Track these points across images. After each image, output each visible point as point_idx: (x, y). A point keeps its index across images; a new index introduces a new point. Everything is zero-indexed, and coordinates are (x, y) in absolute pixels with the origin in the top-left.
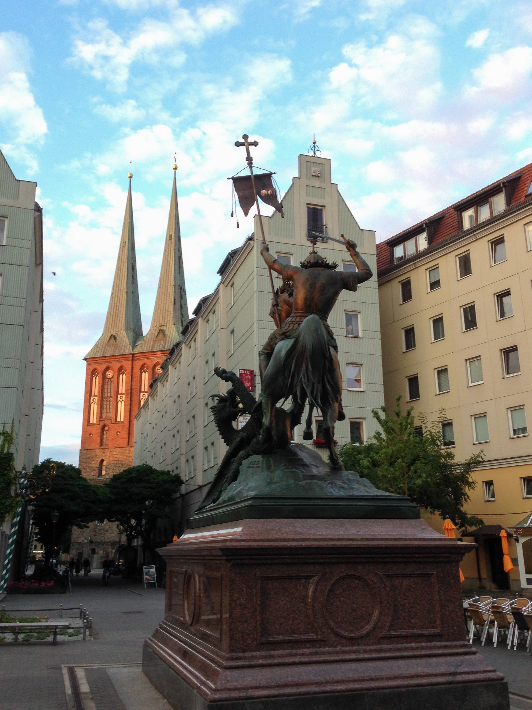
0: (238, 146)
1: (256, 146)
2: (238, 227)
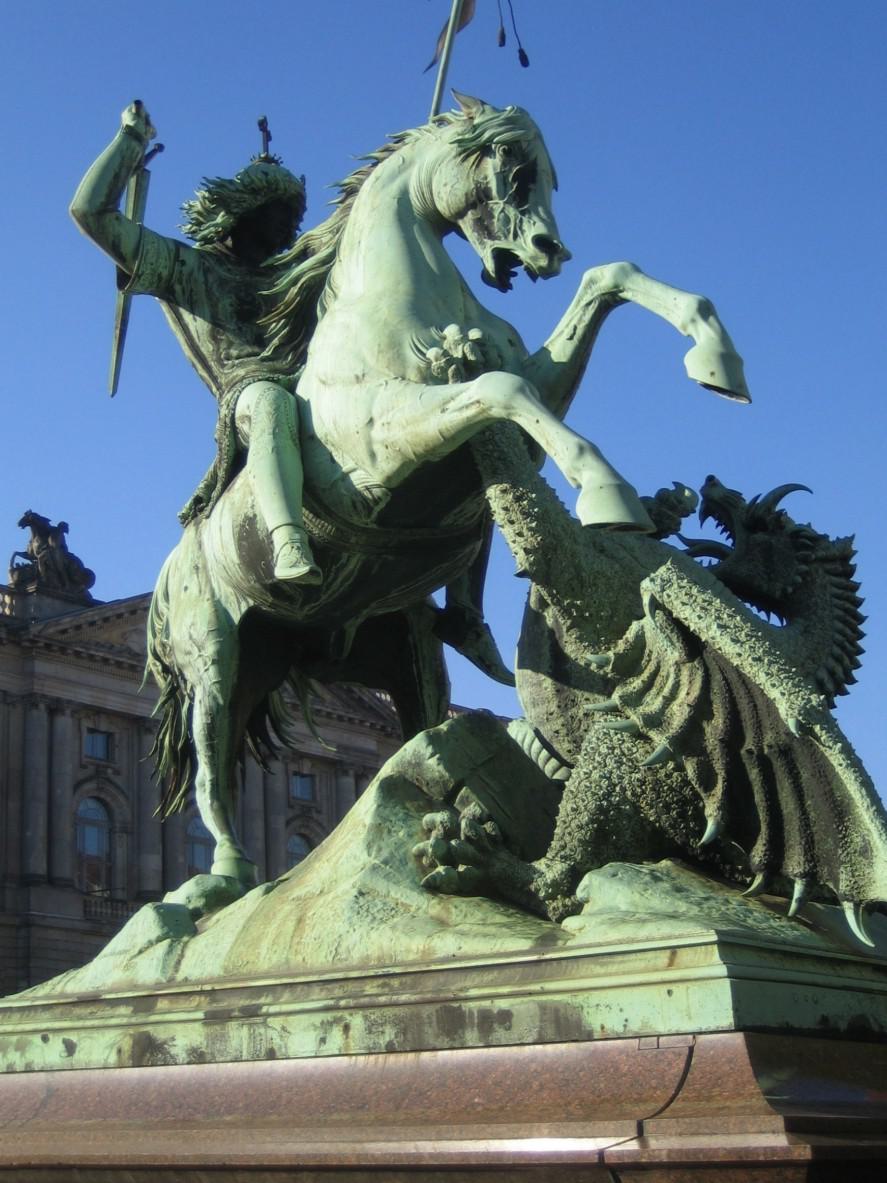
2: (263, 125)
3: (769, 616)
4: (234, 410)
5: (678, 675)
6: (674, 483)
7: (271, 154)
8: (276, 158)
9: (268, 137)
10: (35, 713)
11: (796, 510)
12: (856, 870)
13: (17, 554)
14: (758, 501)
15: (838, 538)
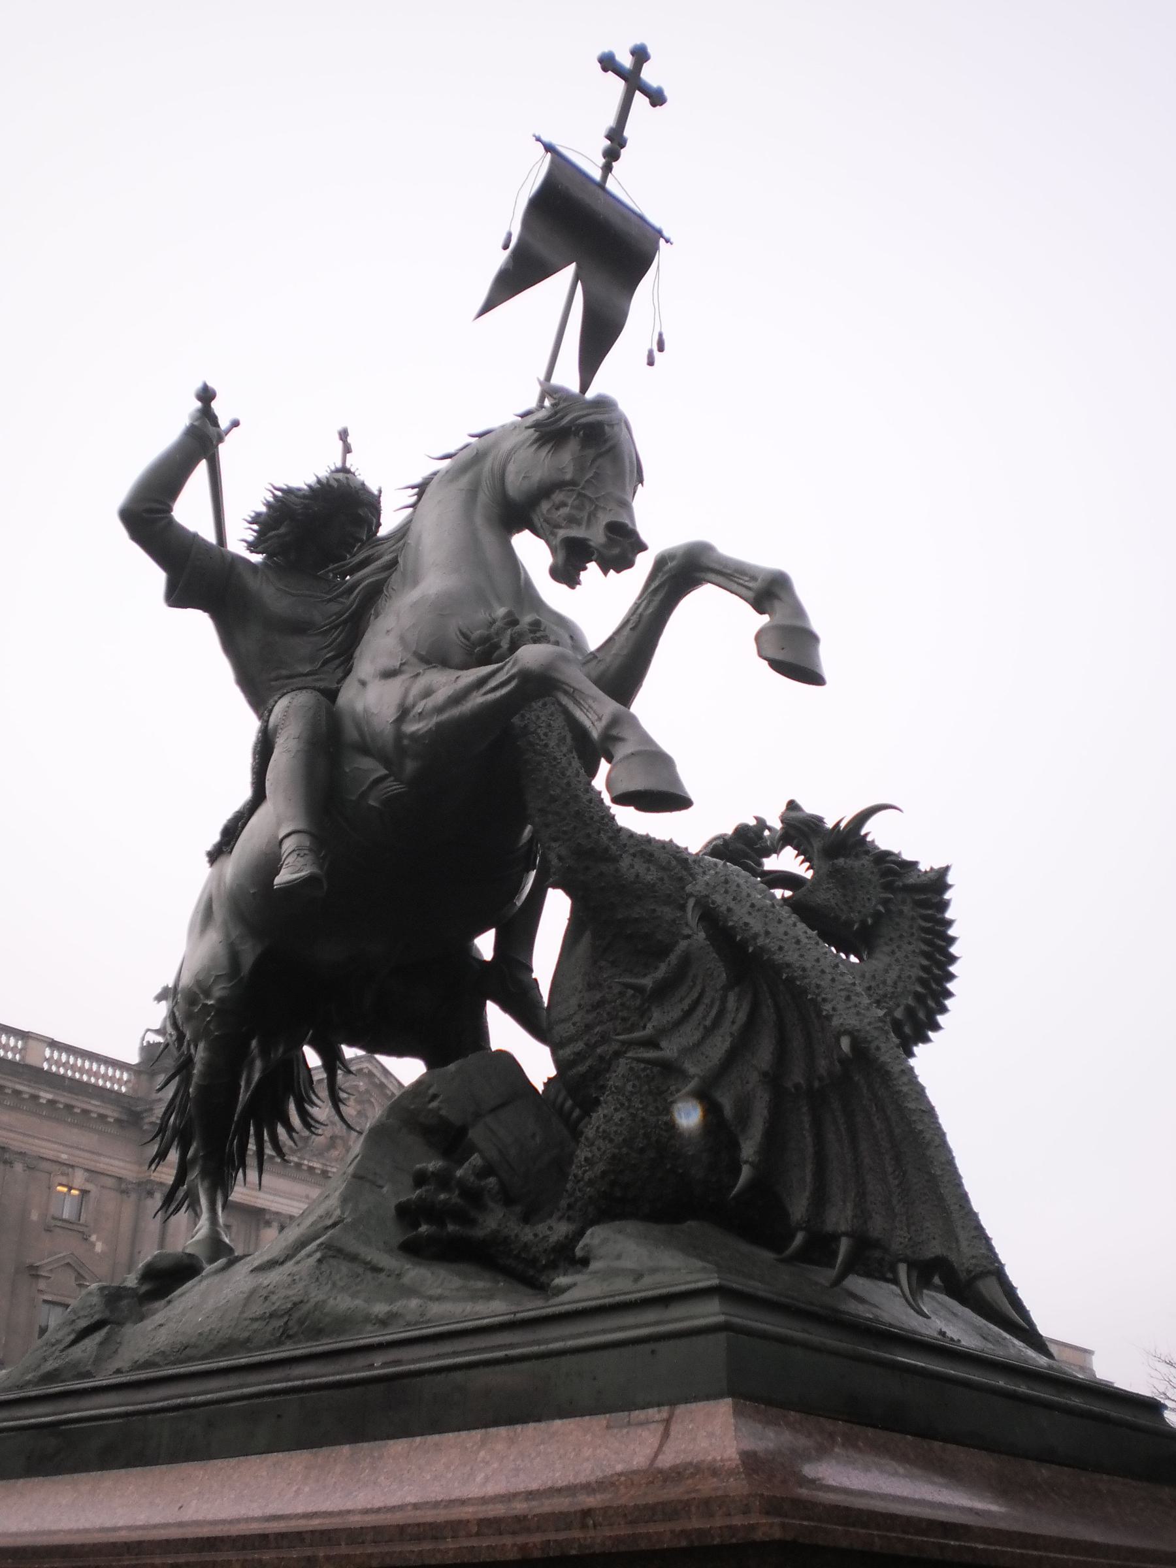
0: (605, 70)
1: (654, 104)
2: (343, 435)
3: (847, 957)
4: (267, 721)
5: (724, 1000)
6: (757, 818)
7: (348, 465)
9: (347, 449)
10: (149, 1202)
11: (882, 834)
12: (914, 1224)
13: (148, 1030)
15: (932, 869)
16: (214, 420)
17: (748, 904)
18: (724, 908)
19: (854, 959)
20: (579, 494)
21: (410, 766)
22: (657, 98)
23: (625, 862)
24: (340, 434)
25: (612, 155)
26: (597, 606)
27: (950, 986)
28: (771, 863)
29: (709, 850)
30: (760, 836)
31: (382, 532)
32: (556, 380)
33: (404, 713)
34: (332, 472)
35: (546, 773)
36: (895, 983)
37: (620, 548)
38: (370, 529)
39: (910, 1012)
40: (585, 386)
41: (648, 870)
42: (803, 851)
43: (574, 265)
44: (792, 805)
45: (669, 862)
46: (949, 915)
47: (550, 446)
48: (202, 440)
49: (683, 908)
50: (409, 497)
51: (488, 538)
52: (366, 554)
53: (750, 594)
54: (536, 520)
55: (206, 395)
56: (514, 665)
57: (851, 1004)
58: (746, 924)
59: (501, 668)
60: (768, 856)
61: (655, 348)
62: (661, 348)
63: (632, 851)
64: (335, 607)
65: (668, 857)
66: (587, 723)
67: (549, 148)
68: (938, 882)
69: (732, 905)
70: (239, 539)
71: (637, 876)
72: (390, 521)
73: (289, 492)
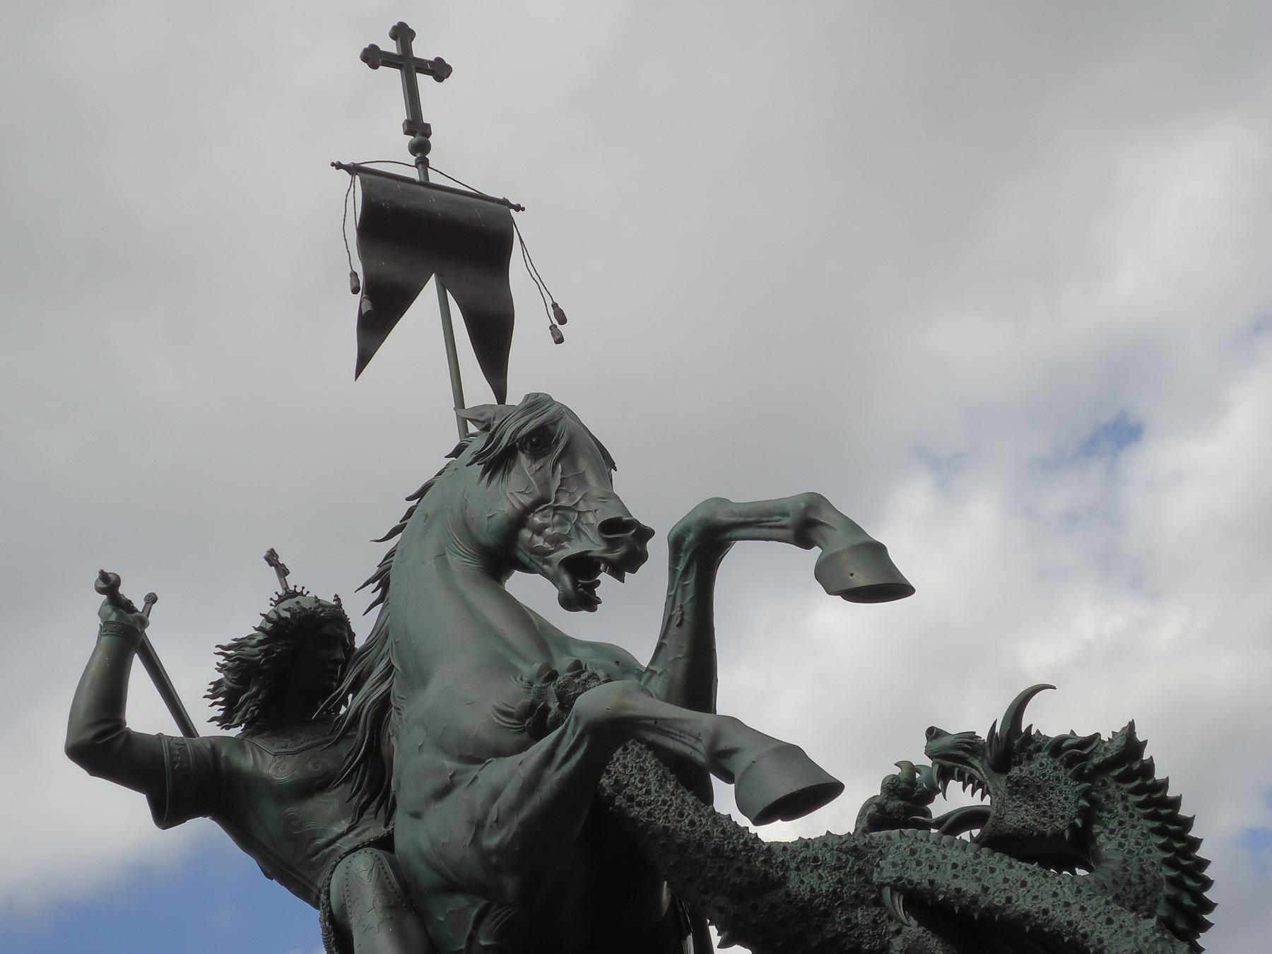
2: (272, 558)
8: (298, 590)
9: (283, 572)
11: (1046, 721)
14: (997, 730)
16: (127, 606)
17: (949, 867)
18: (925, 884)
19: (1081, 872)
20: (556, 509)
21: (510, 884)
22: (440, 70)
23: (792, 883)
24: (267, 559)
25: (421, 149)
26: (630, 619)
27: (1201, 853)
28: (939, 807)
29: (865, 824)
30: (912, 782)
31: (359, 643)
32: (469, 404)
33: (478, 826)
34: (277, 603)
35: (661, 822)
36: (1141, 878)
37: (626, 542)
38: (345, 645)
39: (1174, 902)
40: (501, 394)
41: (820, 877)
42: (966, 780)
43: (433, 278)
44: (933, 733)
45: (839, 859)
46: (1159, 775)
47: (501, 472)
48: (126, 634)
49: (878, 902)
50: (370, 594)
51: (481, 598)
52: (354, 674)
53: (789, 532)
54: (520, 554)
55: (109, 585)
56: (577, 719)
57: (1115, 926)
58: (958, 890)
59: (564, 732)
60: (931, 800)
61: (556, 322)
62: (563, 320)
63: (793, 865)
64: (344, 749)
65: (846, 853)
66: (687, 750)
67: (353, 169)
68: (1130, 746)
69: (932, 875)
70: (205, 719)
71: (812, 890)
72: (362, 629)
73: (240, 644)
